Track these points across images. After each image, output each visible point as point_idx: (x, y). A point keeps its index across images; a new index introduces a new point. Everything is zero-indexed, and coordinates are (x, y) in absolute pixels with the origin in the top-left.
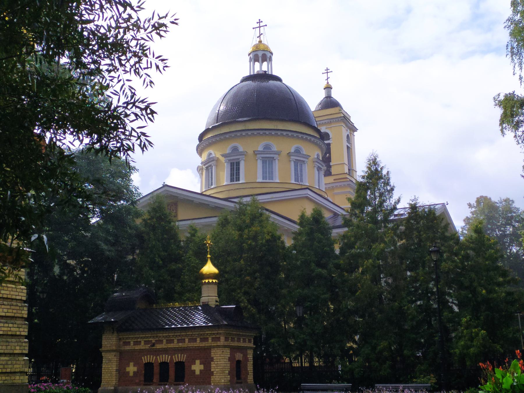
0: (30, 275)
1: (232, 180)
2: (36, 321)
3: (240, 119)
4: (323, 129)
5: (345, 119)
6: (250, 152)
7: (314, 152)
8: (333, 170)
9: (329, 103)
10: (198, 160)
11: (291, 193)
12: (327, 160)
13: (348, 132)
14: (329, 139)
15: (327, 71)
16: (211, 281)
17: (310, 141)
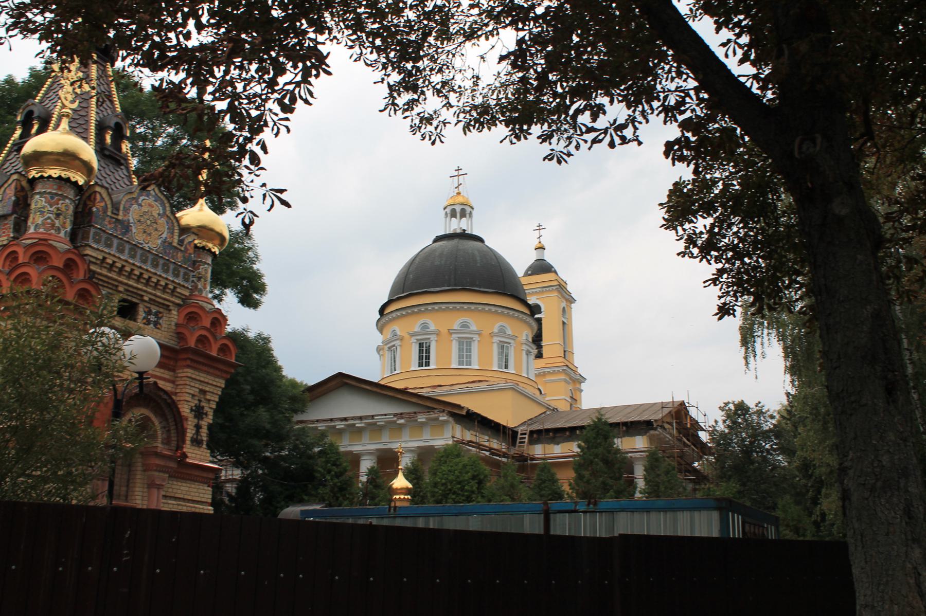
0: (243, 485)
1: (420, 365)
2: (13, 567)
3: (432, 290)
4: (532, 300)
5: (561, 288)
6: (444, 331)
7: (526, 334)
8: (545, 351)
9: (541, 267)
10: (378, 339)
11: (472, 358)
12: (537, 339)
13: (564, 304)
14: (540, 312)
15: (540, 228)
16: (402, 497)
17: (517, 318)
